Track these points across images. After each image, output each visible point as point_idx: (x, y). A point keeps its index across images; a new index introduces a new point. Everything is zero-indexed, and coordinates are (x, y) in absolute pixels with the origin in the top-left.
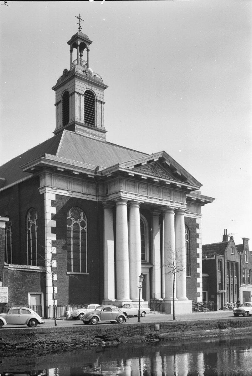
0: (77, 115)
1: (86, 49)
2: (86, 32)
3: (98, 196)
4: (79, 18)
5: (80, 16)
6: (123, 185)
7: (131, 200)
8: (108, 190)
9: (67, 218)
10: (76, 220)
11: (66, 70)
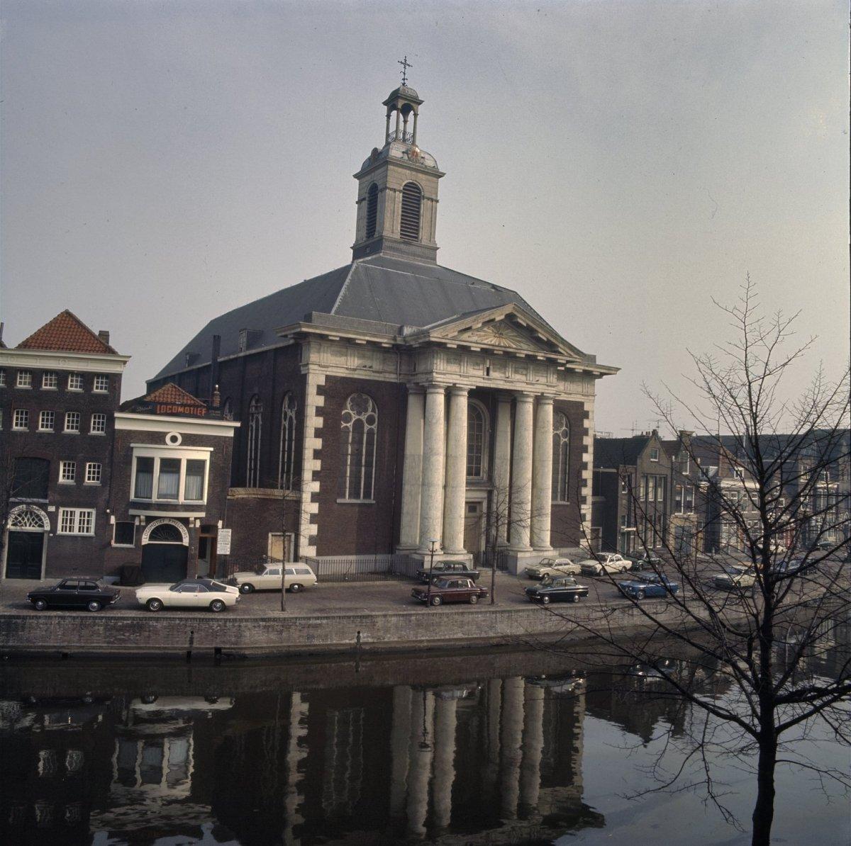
0: (387, 225)
1: (412, 112)
2: (416, 86)
3: (400, 374)
4: (405, 64)
5: (405, 60)
6: (439, 360)
7: (451, 385)
8: (417, 364)
9: (343, 412)
11: (375, 150)
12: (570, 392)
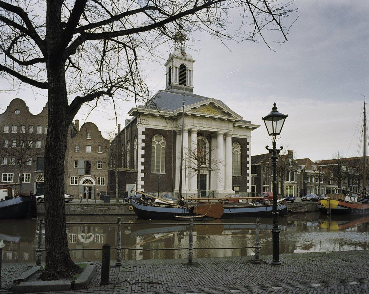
9: (152, 141)
10: (158, 142)
12: (239, 134)
